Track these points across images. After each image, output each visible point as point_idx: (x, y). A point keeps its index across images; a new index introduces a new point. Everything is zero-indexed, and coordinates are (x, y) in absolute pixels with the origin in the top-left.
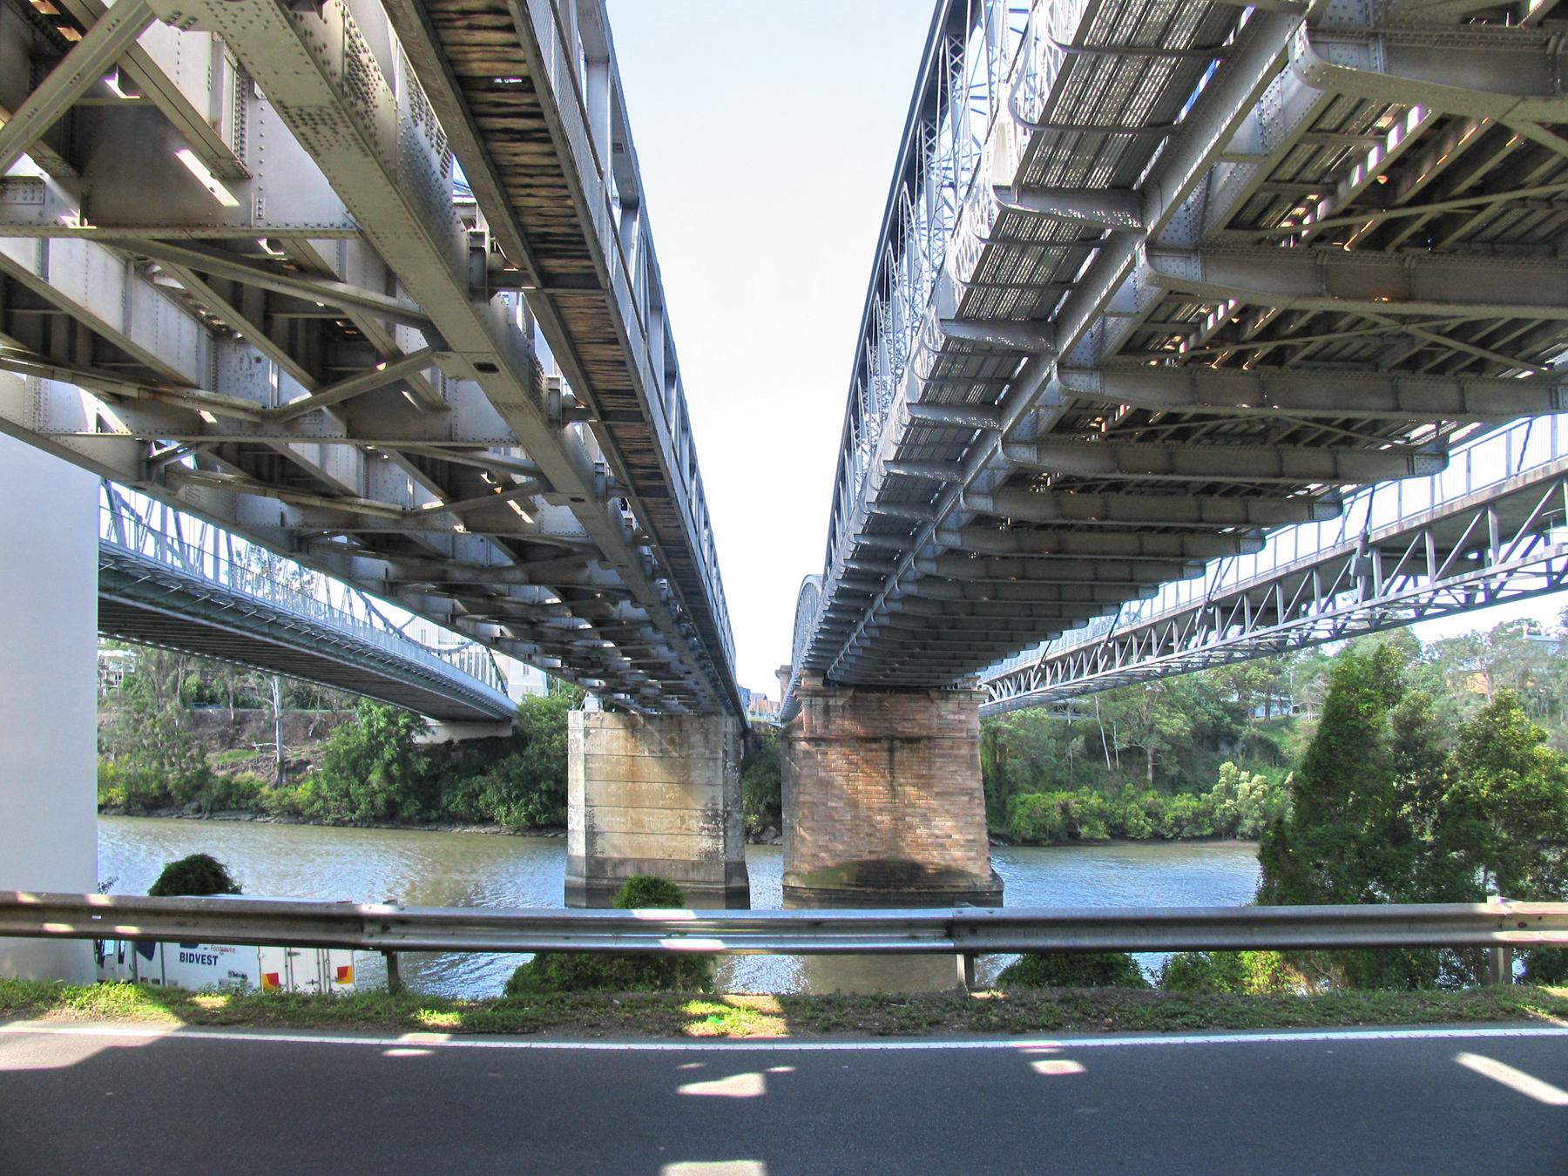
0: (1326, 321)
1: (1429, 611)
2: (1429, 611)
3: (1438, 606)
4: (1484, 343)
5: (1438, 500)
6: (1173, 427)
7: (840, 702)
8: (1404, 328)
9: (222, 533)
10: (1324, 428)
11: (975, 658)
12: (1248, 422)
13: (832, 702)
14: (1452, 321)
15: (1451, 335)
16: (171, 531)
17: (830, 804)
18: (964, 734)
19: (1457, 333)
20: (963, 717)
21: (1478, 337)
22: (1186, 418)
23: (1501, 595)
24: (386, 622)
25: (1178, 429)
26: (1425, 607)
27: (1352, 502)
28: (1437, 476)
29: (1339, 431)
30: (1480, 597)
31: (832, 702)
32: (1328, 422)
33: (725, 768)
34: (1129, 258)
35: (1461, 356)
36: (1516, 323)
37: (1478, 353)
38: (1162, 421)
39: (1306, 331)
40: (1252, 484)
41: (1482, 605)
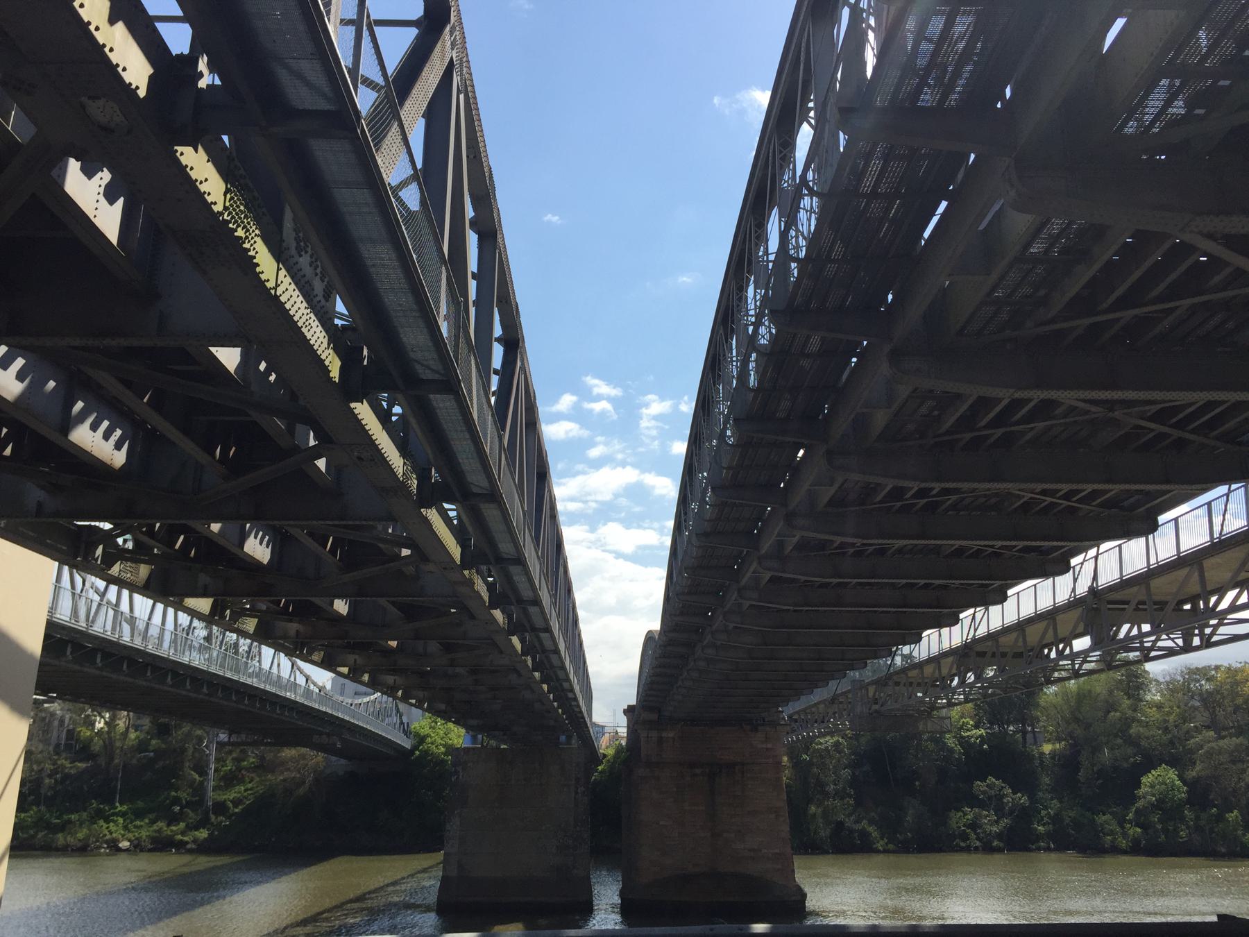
0: (1046, 407)
1: (1153, 654)
2: (1153, 654)
3: (1161, 649)
4: (1179, 425)
5: (1153, 561)
6: (924, 501)
7: (671, 735)
8: (1111, 414)
9: (171, 611)
10: (1049, 499)
11: (313, 919)
12: (985, 496)
13: (664, 734)
14: (1152, 407)
15: (1150, 419)
16: (124, 606)
17: (661, 823)
18: (771, 760)
19: (1159, 417)
20: (769, 746)
21: (1174, 420)
22: (934, 492)
23: (1215, 638)
24: (308, 679)
25: (927, 502)
26: (1152, 649)
27: (1096, 558)
28: (1151, 537)
29: (1152, 425)
30: (1196, 641)
31: (664, 734)
32: (1052, 493)
33: (577, 793)
34: (846, 12)
35: (1162, 436)
36: (1211, 405)
37: (1176, 433)
38: (914, 496)
39: (1030, 418)
40: (992, 547)
41: (1198, 648)
